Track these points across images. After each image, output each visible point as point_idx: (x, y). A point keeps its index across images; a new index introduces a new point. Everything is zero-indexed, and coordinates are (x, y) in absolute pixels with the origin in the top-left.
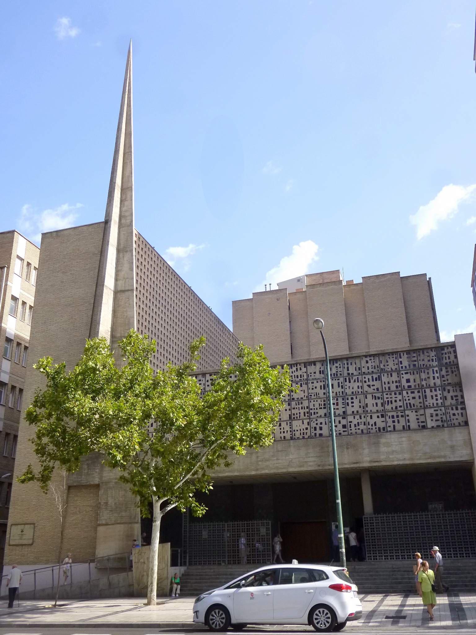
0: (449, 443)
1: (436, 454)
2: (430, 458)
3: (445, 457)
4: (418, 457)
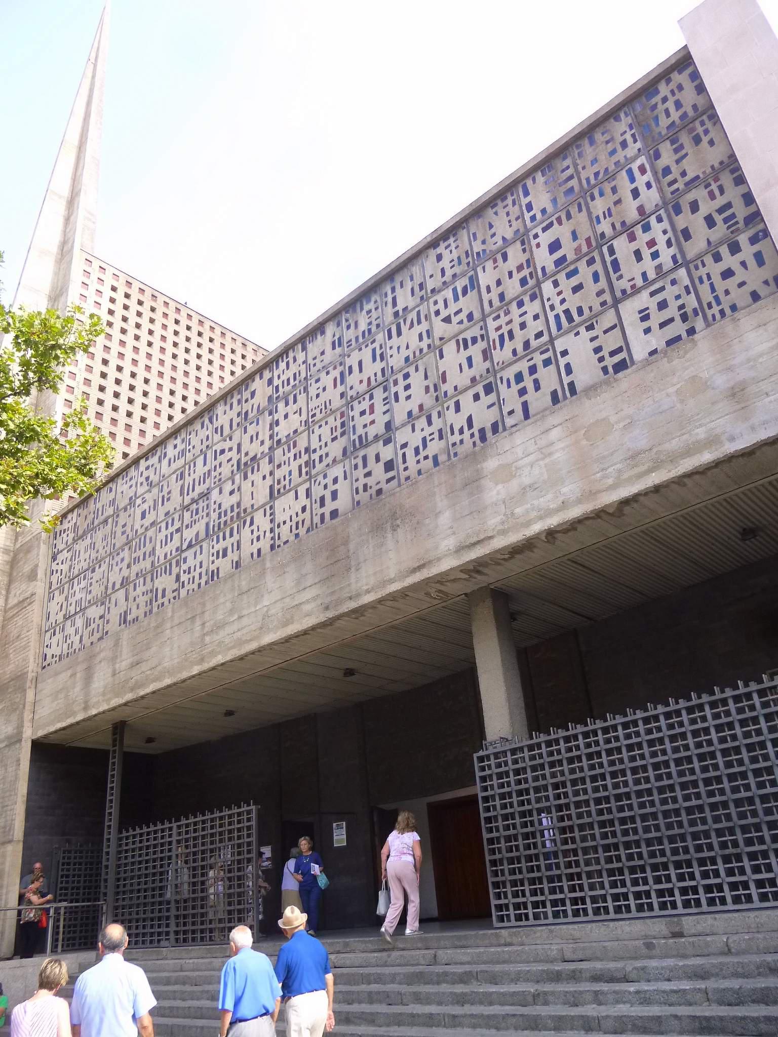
0: (721, 381)
1: (674, 444)
3: (712, 441)
4: (610, 481)
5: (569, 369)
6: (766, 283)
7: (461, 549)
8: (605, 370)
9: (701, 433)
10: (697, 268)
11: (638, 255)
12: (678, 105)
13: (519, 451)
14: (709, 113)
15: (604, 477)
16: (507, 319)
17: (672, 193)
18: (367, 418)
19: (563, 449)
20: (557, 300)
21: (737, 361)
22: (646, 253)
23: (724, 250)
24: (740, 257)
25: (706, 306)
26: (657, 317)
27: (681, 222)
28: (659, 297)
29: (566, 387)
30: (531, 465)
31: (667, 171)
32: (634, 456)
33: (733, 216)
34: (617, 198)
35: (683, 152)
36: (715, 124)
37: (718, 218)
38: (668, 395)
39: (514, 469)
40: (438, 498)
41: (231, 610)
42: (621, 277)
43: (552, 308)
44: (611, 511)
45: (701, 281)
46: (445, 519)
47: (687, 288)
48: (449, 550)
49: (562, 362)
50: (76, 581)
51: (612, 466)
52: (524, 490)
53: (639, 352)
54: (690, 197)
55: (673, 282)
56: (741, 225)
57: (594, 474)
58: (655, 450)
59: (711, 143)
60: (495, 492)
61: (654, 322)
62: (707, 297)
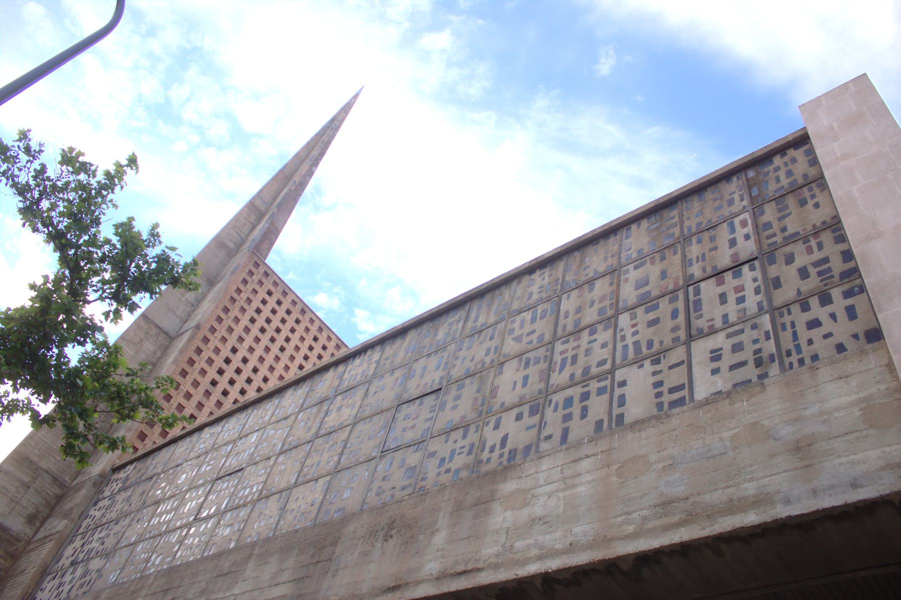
0: (786, 432)
1: (717, 497)
2: (689, 519)
3: (760, 500)
4: (631, 529)
5: (622, 401)
6: (856, 336)
7: (442, 576)
8: (660, 406)
9: (750, 489)
10: (782, 315)
11: (723, 298)
12: (789, 174)
13: (542, 478)
14: (820, 181)
15: (623, 523)
16: (575, 344)
17: (769, 245)
18: (409, 423)
19: (588, 482)
20: (628, 333)
21: (808, 413)
22: (732, 297)
23: (814, 302)
24: (829, 309)
25: (784, 354)
26: (728, 359)
27: (773, 271)
28: (735, 340)
29: (614, 418)
30: (550, 495)
31: (768, 225)
32: (666, 504)
33: (829, 270)
34: (714, 246)
35: (787, 212)
36: (823, 190)
37: (813, 271)
38: (721, 439)
39: (530, 496)
40: (441, 514)
41: (202, 591)
42: (701, 316)
43: (623, 338)
44: (625, 567)
45: (784, 328)
46: (439, 539)
47: (767, 333)
48: (431, 574)
49: (618, 392)
50: (99, 529)
51: (638, 510)
52: (533, 521)
53: (701, 392)
54: (787, 249)
55: (754, 327)
56: (836, 278)
57: (615, 517)
58: (692, 500)
59: (817, 205)
60: (501, 519)
61: (724, 364)
62: (787, 341)
